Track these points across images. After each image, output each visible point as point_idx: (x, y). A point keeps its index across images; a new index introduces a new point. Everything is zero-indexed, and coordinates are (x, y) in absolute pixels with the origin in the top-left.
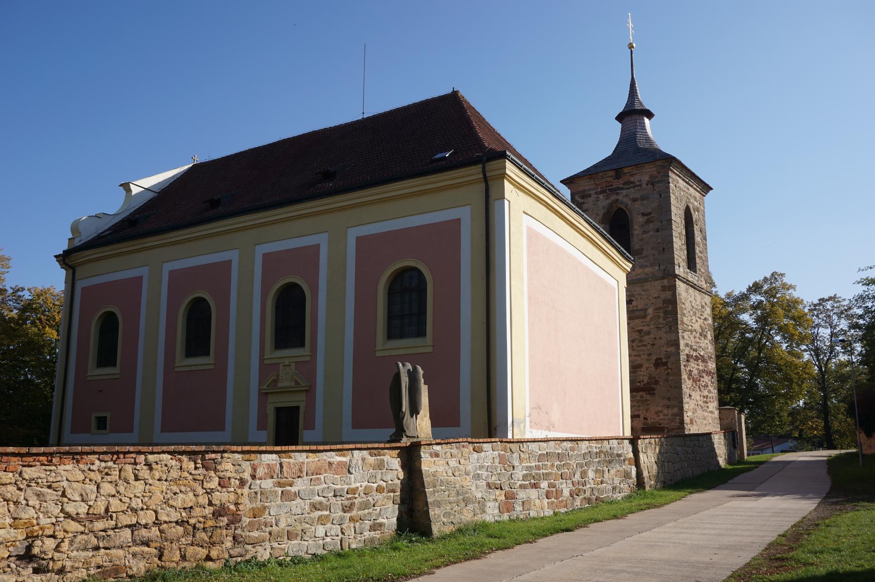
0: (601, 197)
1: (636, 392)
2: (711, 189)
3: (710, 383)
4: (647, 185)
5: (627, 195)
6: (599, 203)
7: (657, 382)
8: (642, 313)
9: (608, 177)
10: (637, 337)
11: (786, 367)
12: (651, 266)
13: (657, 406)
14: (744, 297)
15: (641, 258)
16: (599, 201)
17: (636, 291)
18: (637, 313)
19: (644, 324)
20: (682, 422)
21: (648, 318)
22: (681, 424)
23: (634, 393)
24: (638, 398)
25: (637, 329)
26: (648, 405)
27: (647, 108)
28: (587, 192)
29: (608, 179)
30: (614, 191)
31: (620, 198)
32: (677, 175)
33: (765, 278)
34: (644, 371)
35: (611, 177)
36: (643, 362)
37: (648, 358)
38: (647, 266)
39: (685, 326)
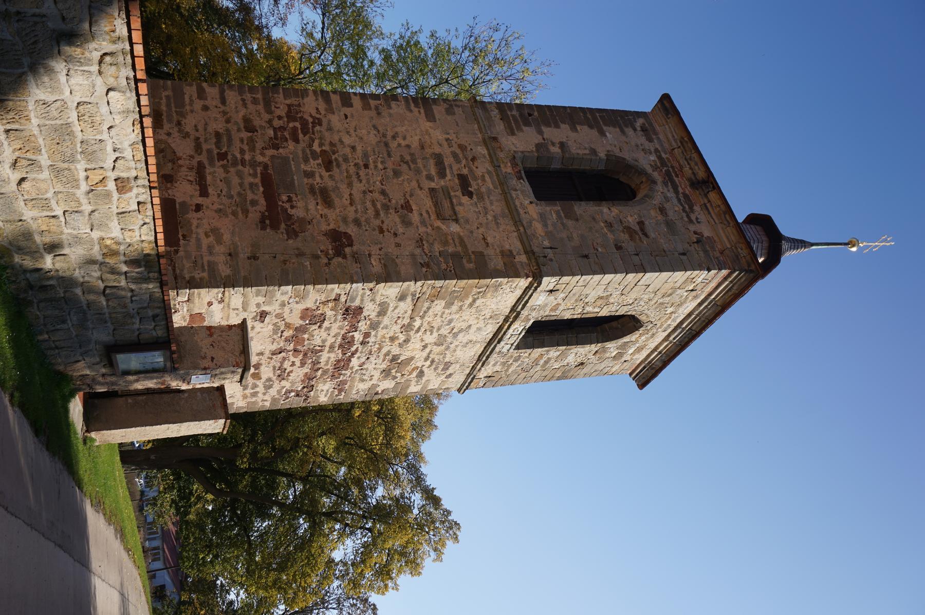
0: (653, 158)
1: (263, 192)
2: (642, 386)
3: (287, 384)
4: (695, 233)
5: (667, 199)
6: (642, 153)
7: (292, 233)
8: (447, 212)
9: (691, 168)
10: (394, 201)
11: (307, 557)
12: (546, 233)
13: (233, 233)
14: (418, 481)
15: (559, 217)
16: (645, 153)
17: (491, 204)
18: (446, 204)
19: (425, 214)
20: (194, 284)
21: (438, 223)
22: (188, 282)
23: (261, 189)
24: (250, 196)
25: (411, 202)
26: (234, 214)
27: (783, 259)
28: (654, 137)
29: (687, 169)
30: (669, 179)
31: (660, 187)
32: (710, 294)
33: (449, 513)
34: (317, 210)
35: (693, 173)
36: (338, 210)
37: (350, 220)
38: (545, 225)
39: (426, 305)
